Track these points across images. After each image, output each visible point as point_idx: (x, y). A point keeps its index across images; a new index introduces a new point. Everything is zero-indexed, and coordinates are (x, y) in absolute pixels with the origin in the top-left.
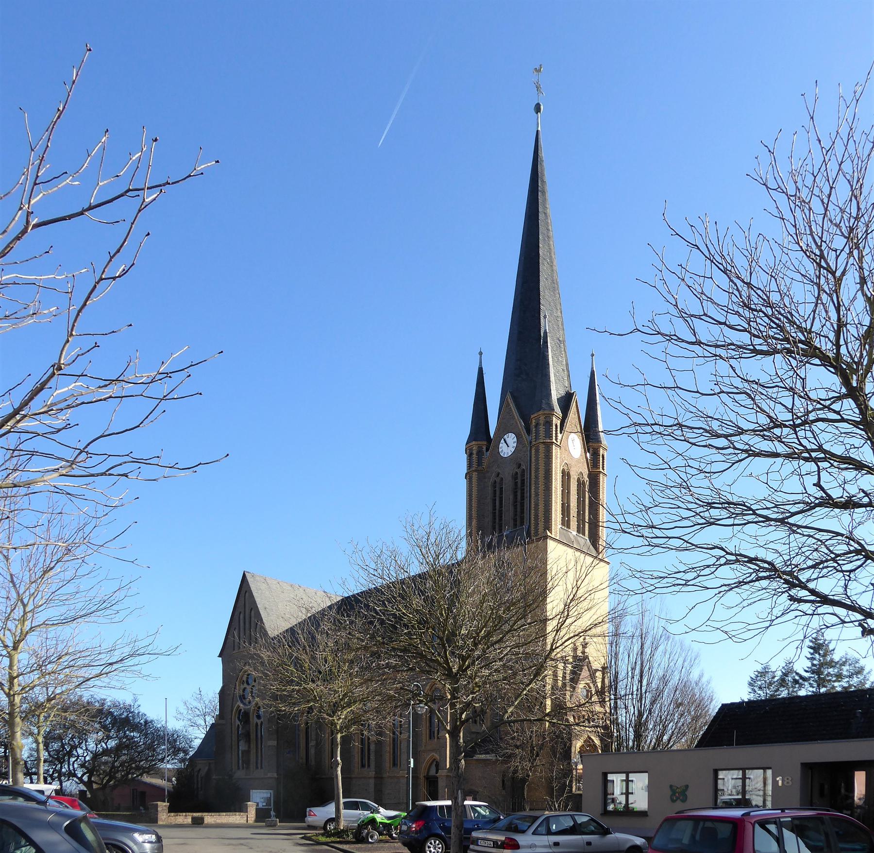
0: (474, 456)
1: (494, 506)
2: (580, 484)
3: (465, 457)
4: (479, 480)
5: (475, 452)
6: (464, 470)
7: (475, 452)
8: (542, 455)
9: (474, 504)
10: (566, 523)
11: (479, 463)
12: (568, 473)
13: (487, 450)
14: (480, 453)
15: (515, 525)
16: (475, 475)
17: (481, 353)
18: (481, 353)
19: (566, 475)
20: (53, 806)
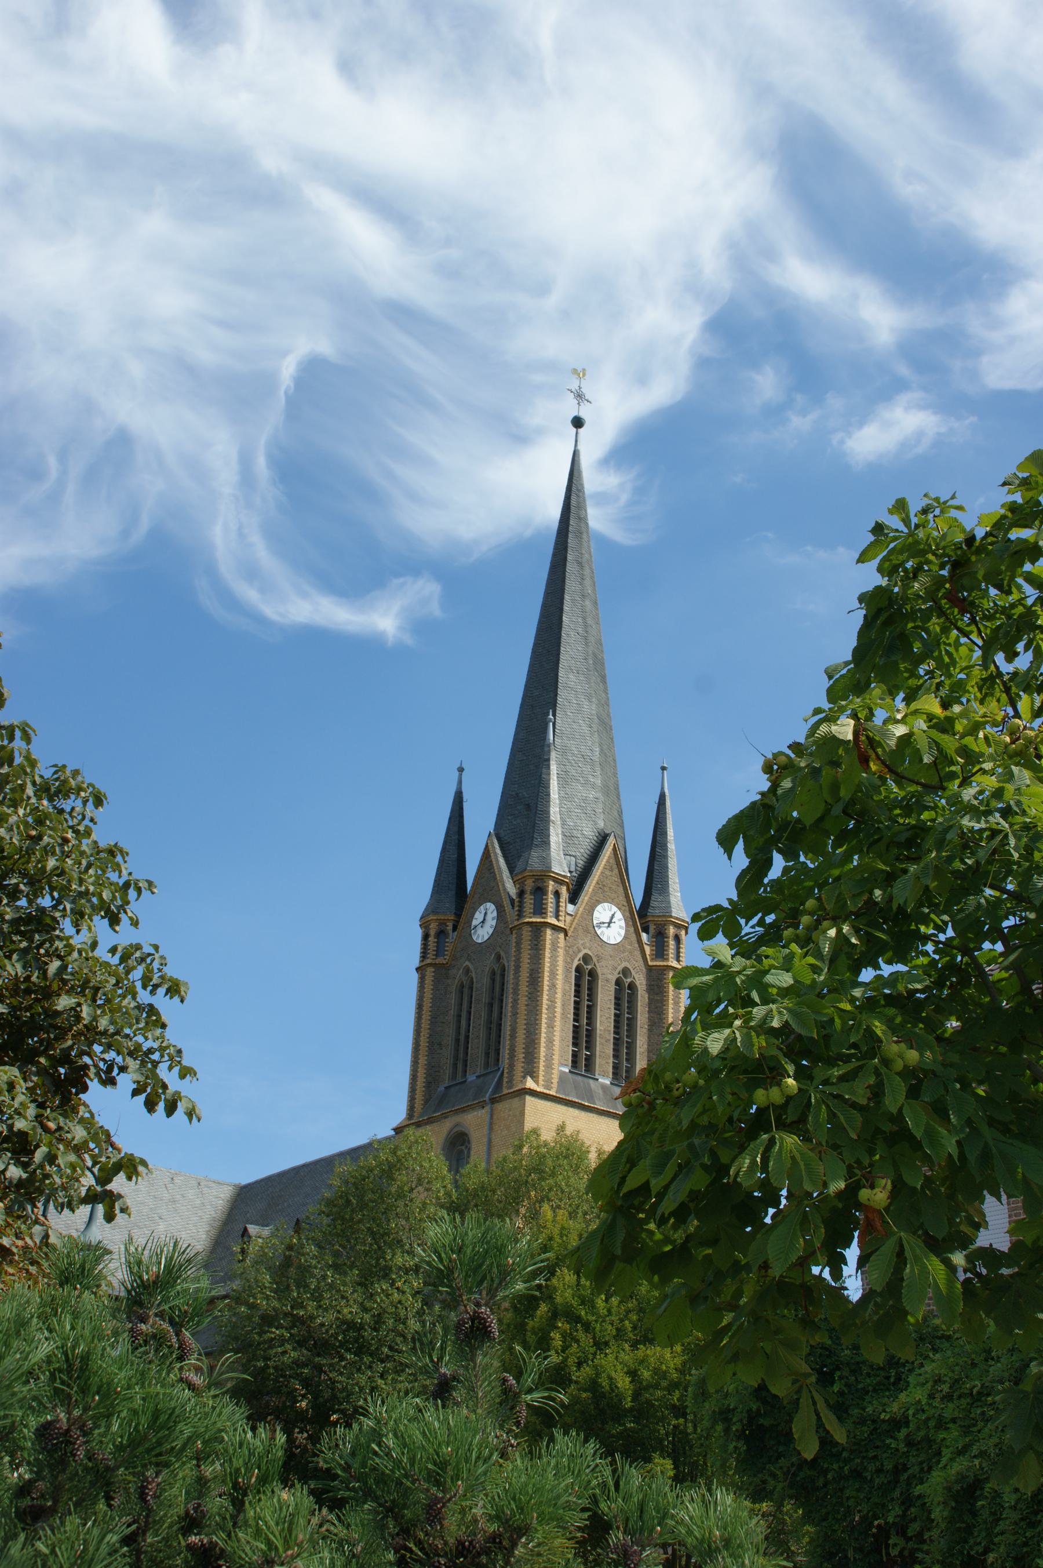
0: (431, 939)
1: (459, 1028)
2: (625, 992)
3: (419, 933)
4: (437, 981)
5: (432, 933)
6: (416, 962)
7: (432, 933)
8: (524, 975)
9: (425, 1025)
10: (582, 1061)
11: (438, 953)
12: (592, 974)
13: (455, 928)
14: (441, 933)
15: (487, 1065)
16: (430, 972)
17: (461, 770)
18: (461, 770)
19: (585, 980)
20: (677, 1003)
